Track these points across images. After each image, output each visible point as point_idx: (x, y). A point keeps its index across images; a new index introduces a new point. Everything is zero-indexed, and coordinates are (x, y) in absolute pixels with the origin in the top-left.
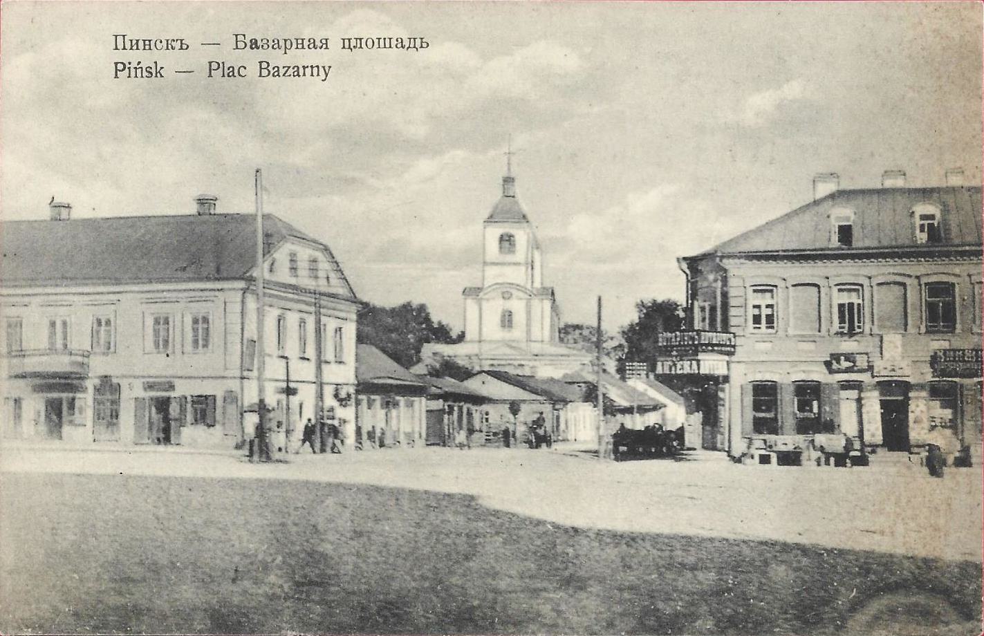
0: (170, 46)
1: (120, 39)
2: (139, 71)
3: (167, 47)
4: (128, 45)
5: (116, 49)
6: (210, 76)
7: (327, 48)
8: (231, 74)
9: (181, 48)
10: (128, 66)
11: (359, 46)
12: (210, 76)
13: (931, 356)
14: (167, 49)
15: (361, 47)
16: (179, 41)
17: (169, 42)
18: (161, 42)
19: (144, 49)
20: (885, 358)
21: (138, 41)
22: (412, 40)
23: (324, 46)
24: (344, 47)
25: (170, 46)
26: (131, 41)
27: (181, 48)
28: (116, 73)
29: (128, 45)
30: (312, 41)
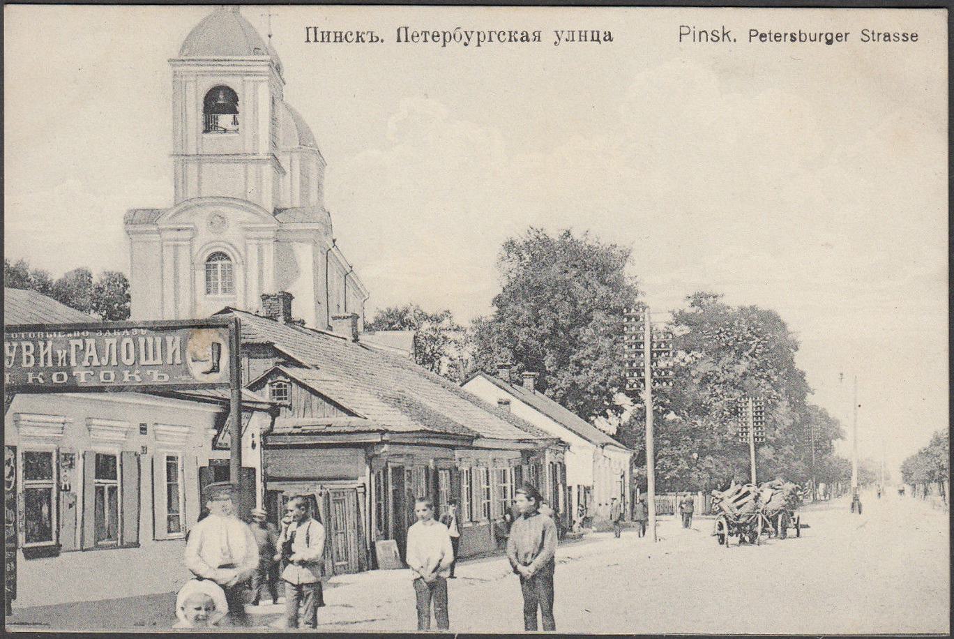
0: (513, 39)
1: (312, 31)
2: (703, 35)
3: (407, 38)
4: (319, 38)
5: (308, 41)
6: (479, 45)
7: (539, 40)
8: (524, 39)
9: (372, 41)
10: (692, 30)
11: (571, 39)
12: (479, 45)
13: (303, 567)
14: (510, 40)
15: (573, 40)
16: (370, 34)
17: (512, 34)
18: (504, 34)
19: (335, 41)
20: (188, 571)
21: (329, 33)
22: (595, 39)
23: (537, 38)
24: (308, 41)
25: (513, 39)
26: (323, 32)
27: (372, 41)
28: (479, 43)
29: (319, 38)
30: (525, 34)
